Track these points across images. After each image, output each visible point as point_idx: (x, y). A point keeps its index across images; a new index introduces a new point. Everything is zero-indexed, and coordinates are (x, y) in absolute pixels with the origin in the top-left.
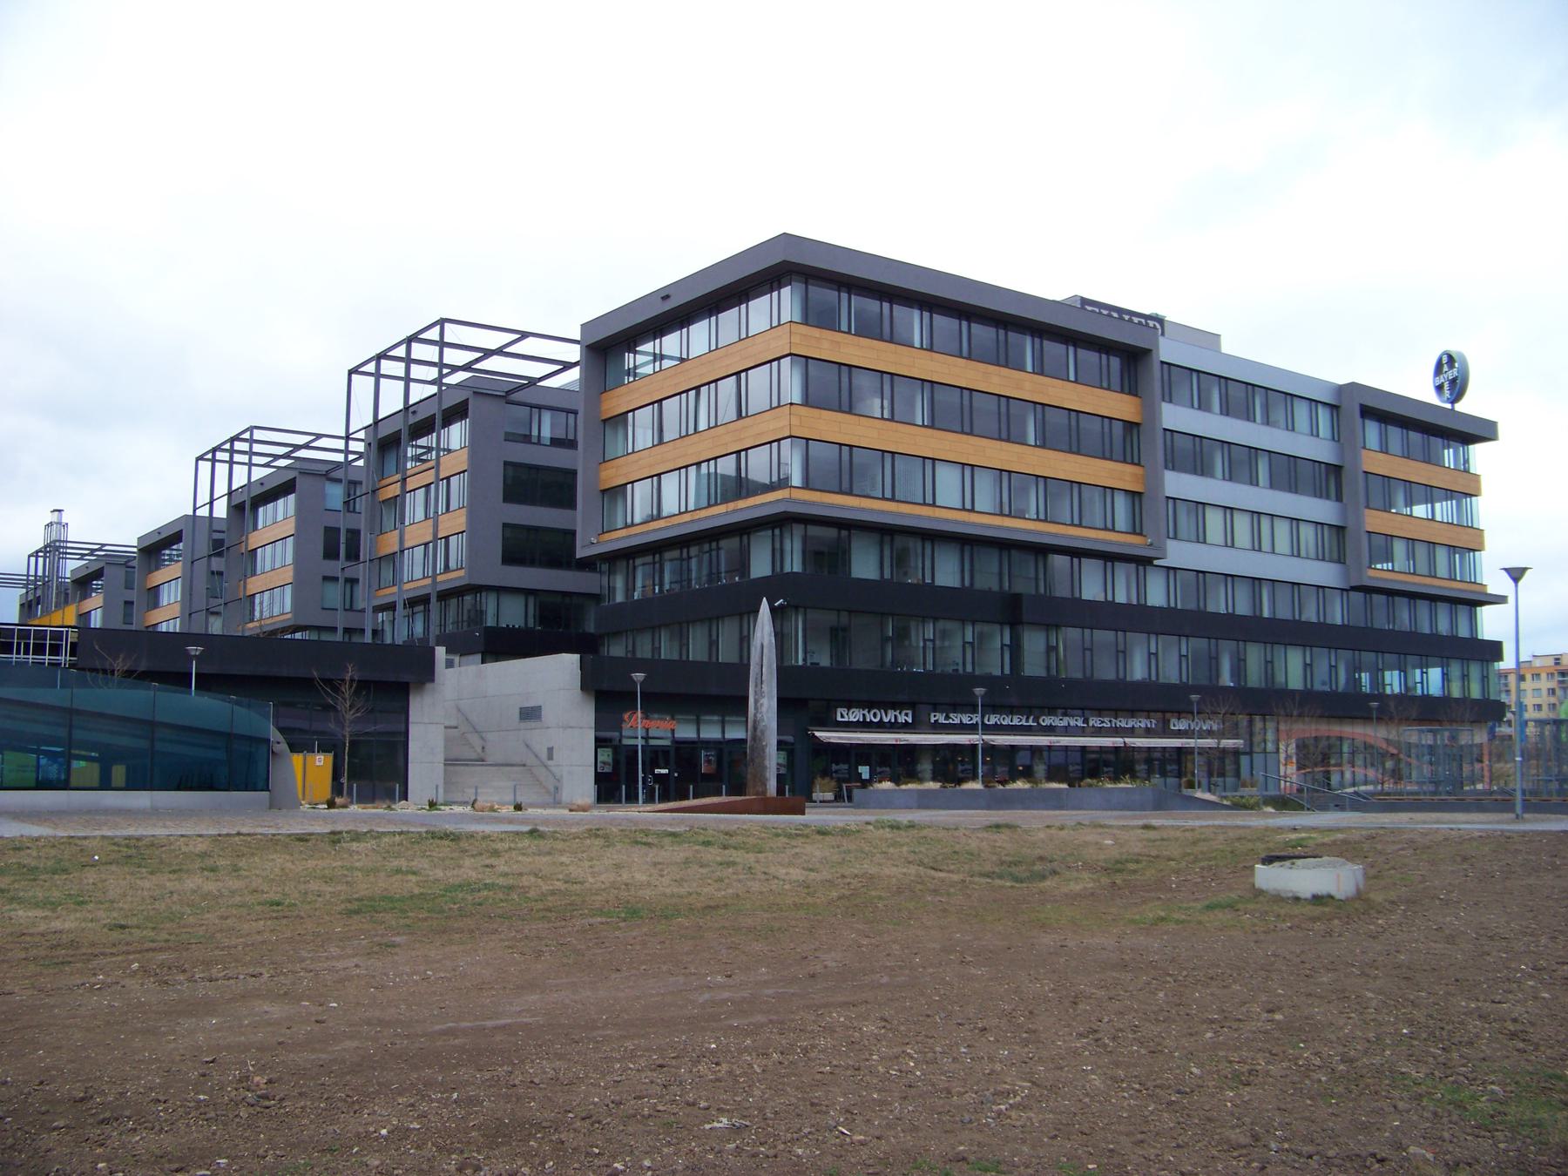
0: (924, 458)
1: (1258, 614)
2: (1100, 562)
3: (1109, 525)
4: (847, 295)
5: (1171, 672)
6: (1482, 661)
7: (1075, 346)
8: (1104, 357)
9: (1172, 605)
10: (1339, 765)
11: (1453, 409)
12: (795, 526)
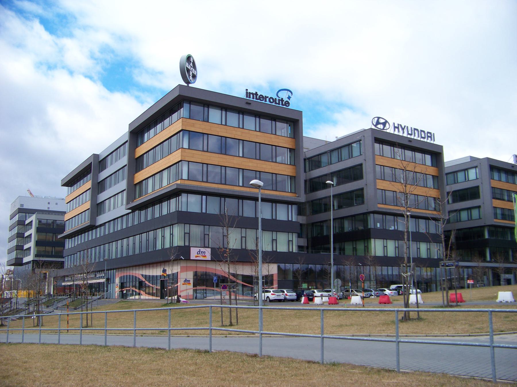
0: (256, 171)
1: (385, 228)
2: (286, 206)
3: (427, 209)
4: (207, 108)
5: (391, 252)
6: (427, 242)
7: (226, 111)
8: (381, 145)
9: (290, 219)
10: (110, 284)
11: (188, 86)
12: (183, 194)
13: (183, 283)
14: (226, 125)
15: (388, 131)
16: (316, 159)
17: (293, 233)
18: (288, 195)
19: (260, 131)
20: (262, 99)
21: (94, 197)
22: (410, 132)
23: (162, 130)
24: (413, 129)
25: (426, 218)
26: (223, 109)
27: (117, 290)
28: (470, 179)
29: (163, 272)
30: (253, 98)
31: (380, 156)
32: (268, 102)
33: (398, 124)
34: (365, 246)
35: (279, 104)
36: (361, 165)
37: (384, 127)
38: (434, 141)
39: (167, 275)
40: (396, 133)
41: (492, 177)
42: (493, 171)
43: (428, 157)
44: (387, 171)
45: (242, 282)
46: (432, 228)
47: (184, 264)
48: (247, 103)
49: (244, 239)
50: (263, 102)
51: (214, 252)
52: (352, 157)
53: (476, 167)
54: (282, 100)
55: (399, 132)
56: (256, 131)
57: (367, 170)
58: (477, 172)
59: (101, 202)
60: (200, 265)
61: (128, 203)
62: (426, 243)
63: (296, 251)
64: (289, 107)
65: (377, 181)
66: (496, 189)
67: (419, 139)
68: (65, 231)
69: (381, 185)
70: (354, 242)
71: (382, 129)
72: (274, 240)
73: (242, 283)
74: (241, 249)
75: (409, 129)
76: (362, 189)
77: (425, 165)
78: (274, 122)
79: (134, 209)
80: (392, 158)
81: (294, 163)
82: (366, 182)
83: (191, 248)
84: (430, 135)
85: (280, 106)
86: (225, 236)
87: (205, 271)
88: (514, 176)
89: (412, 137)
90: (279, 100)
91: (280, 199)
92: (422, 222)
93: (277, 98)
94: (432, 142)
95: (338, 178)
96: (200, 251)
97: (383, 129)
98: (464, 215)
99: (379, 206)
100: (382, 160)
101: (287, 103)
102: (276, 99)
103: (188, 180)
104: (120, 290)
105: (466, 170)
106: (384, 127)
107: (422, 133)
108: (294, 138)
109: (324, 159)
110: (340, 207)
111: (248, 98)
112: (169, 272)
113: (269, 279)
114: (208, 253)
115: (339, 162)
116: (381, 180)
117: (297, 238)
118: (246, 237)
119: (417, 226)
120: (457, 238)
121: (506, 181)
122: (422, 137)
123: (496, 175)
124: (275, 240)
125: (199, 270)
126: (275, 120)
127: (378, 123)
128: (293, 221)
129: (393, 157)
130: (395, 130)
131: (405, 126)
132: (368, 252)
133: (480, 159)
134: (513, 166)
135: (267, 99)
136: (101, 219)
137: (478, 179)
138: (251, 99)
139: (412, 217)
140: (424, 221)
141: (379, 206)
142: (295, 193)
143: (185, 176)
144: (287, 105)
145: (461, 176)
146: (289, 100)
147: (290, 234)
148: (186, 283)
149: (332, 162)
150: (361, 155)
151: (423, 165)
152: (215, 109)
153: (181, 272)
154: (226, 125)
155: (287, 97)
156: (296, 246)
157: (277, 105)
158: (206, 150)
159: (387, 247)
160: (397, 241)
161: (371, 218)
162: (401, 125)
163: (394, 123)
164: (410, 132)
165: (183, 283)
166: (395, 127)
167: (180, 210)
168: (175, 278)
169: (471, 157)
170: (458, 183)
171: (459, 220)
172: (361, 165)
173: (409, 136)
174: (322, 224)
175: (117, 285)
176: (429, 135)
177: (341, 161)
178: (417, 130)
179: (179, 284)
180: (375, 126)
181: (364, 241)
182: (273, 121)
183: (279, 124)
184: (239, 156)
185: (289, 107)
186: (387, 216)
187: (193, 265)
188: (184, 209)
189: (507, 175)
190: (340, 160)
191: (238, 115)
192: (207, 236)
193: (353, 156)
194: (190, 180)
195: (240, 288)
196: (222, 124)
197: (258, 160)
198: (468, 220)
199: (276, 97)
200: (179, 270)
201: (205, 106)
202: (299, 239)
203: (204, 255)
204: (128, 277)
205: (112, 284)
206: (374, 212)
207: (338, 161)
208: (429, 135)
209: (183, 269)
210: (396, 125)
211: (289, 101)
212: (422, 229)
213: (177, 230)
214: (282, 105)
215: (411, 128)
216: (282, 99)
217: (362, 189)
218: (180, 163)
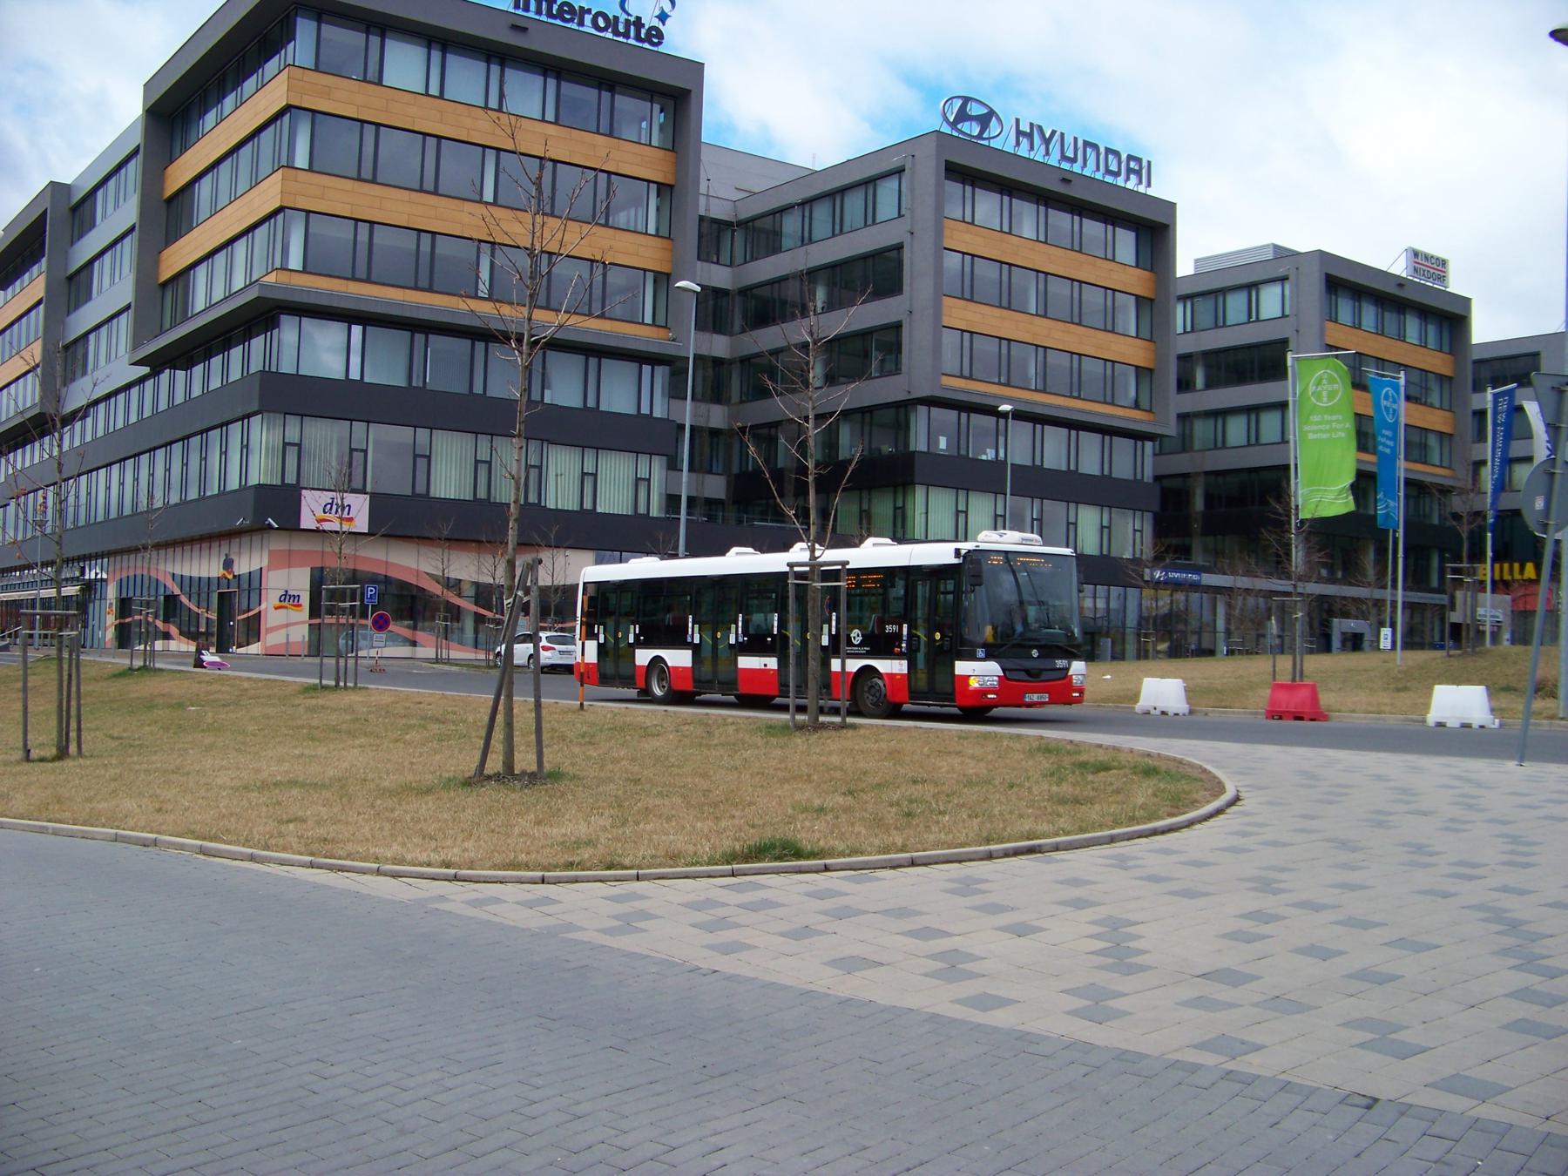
13: (277, 603)
14: (441, 97)
15: (994, 144)
16: (767, 223)
17: (637, 453)
18: (641, 335)
19: (556, 123)
20: (568, 17)
21: (54, 323)
22: (1070, 154)
23: (238, 104)
24: (1080, 144)
25: (1108, 431)
26: (433, 45)
27: (111, 620)
28: (1263, 316)
29: (224, 568)
30: (539, 12)
31: (964, 221)
32: (588, 28)
33: (1032, 125)
34: (895, 509)
35: (628, 37)
36: (899, 247)
37: (982, 131)
38: (1149, 185)
39: (234, 576)
40: (1023, 151)
41: (1402, 332)
42: (1336, 295)
43: (1126, 242)
44: (1059, 289)
45: (476, 604)
46: (1126, 462)
47: (279, 543)
48: (515, 27)
49: (533, 473)
50: (575, 26)
51: (381, 506)
52: (874, 222)
53: (1283, 279)
54: (638, 23)
55: (1032, 148)
56: (543, 120)
57: (916, 264)
58: (1287, 292)
59: (76, 341)
60: (330, 548)
61: (136, 344)
62: (1099, 508)
63: (660, 511)
64: (661, 49)
65: (947, 301)
66: (1386, 363)
67: (1099, 176)
68: (857, 545)
69: (960, 314)
70: (865, 494)
71: (974, 137)
72: (588, 474)
73: (475, 608)
74: (471, 499)
75: (1069, 140)
76: (897, 326)
77: (1113, 260)
78: (606, 95)
79: (158, 363)
80: (1001, 231)
81: (667, 234)
82: (911, 305)
83: (304, 492)
84: (1137, 168)
85: (631, 41)
86: (422, 459)
87: (351, 566)
88: (1404, 315)
89: (1077, 168)
90: (627, 23)
91: (613, 343)
92: (1090, 442)
93: (623, 17)
94: (1141, 189)
95: (831, 285)
96: (332, 504)
97: (980, 136)
98: (1236, 430)
99: (946, 381)
100: (967, 237)
101: (656, 36)
102: (616, 18)
103: (305, 271)
104: (118, 622)
105: (1252, 287)
106: (982, 131)
107: (1111, 157)
108: (673, 150)
109: (791, 225)
110: (831, 379)
111: (520, 12)
112: (243, 566)
113: (554, 600)
114: (360, 510)
115: (834, 235)
116: (963, 298)
117: (664, 472)
118: (595, 475)
119: (1037, 446)
120: (1209, 499)
121: (1377, 328)
122: (1108, 172)
123: (1345, 308)
124: (592, 474)
125: (332, 563)
126: (611, 89)
127: (962, 116)
128: (655, 415)
129: (1006, 229)
130: (1018, 144)
131: (1054, 132)
132: (904, 526)
133: (1295, 254)
134: (1401, 283)
135: (588, 19)
136: (78, 395)
137: (1287, 316)
138: (531, 15)
139: (1018, 415)
140: (1095, 438)
141: (946, 381)
142: (665, 327)
143: (295, 262)
144: (656, 40)
145: (1236, 306)
146: (664, 24)
147: (644, 459)
148: (286, 604)
149: (815, 237)
150: (900, 216)
151: (1106, 259)
152: (398, 40)
153: (270, 568)
154: (441, 97)
155: (657, 12)
156: (660, 494)
157: (621, 39)
158: (431, 188)
159: (1075, 524)
160: (1106, 510)
161: (920, 420)
162: (1040, 128)
163: (1017, 121)
164: (1070, 154)
165: (277, 603)
166: (1019, 133)
167: (274, 369)
168: (253, 585)
169: (1276, 247)
170: (1224, 325)
171: (1219, 444)
172: (899, 247)
173: (1065, 166)
174: (773, 431)
175: (111, 604)
176: (1132, 165)
177: (841, 232)
178: (1095, 147)
179: (263, 606)
180: (953, 125)
181: (895, 493)
182: (603, 93)
183: (625, 103)
184: (646, 234)
185: (661, 49)
186: (972, 415)
187: (314, 546)
188: (287, 367)
189: (1423, 324)
190: (838, 229)
191: (483, 65)
192: (358, 456)
193: (878, 221)
194: (310, 273)
195: (469, 624)
196: (427, 94)
197: (1076, 324)
198: (1249, 445)
199: (619, 12)
200: (265, 563)
201: (493, 60)
202: (669, 472)
203: (345, 515)
204: (195, 584)
205: (97, 603)
206: (931, 402)
207: (830, 235)
208: (1132, 165)
209: (286, 560)
210: (1025, 128)
211: (661, 26)
212: (1090, 464)
213: (263, 434)
214: (638, 38)
215: (1076, 139)
216: (638, 19)
217: (897, 326)
218: (280, 217)
